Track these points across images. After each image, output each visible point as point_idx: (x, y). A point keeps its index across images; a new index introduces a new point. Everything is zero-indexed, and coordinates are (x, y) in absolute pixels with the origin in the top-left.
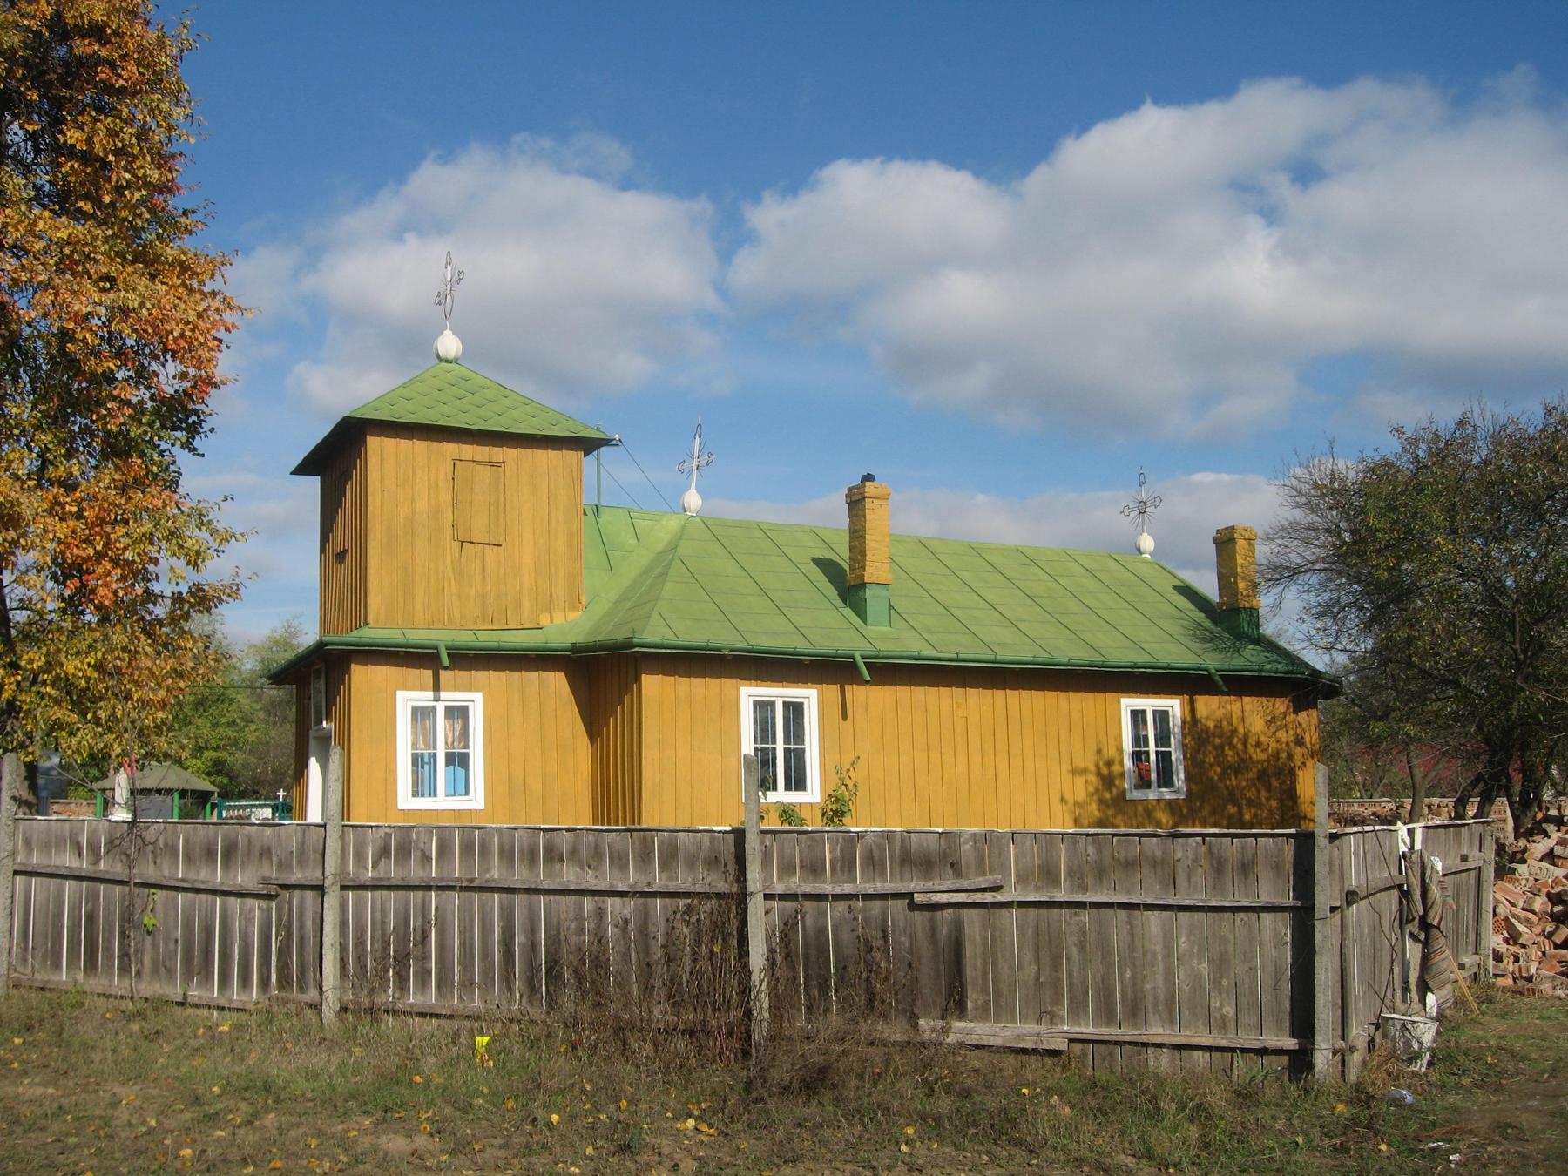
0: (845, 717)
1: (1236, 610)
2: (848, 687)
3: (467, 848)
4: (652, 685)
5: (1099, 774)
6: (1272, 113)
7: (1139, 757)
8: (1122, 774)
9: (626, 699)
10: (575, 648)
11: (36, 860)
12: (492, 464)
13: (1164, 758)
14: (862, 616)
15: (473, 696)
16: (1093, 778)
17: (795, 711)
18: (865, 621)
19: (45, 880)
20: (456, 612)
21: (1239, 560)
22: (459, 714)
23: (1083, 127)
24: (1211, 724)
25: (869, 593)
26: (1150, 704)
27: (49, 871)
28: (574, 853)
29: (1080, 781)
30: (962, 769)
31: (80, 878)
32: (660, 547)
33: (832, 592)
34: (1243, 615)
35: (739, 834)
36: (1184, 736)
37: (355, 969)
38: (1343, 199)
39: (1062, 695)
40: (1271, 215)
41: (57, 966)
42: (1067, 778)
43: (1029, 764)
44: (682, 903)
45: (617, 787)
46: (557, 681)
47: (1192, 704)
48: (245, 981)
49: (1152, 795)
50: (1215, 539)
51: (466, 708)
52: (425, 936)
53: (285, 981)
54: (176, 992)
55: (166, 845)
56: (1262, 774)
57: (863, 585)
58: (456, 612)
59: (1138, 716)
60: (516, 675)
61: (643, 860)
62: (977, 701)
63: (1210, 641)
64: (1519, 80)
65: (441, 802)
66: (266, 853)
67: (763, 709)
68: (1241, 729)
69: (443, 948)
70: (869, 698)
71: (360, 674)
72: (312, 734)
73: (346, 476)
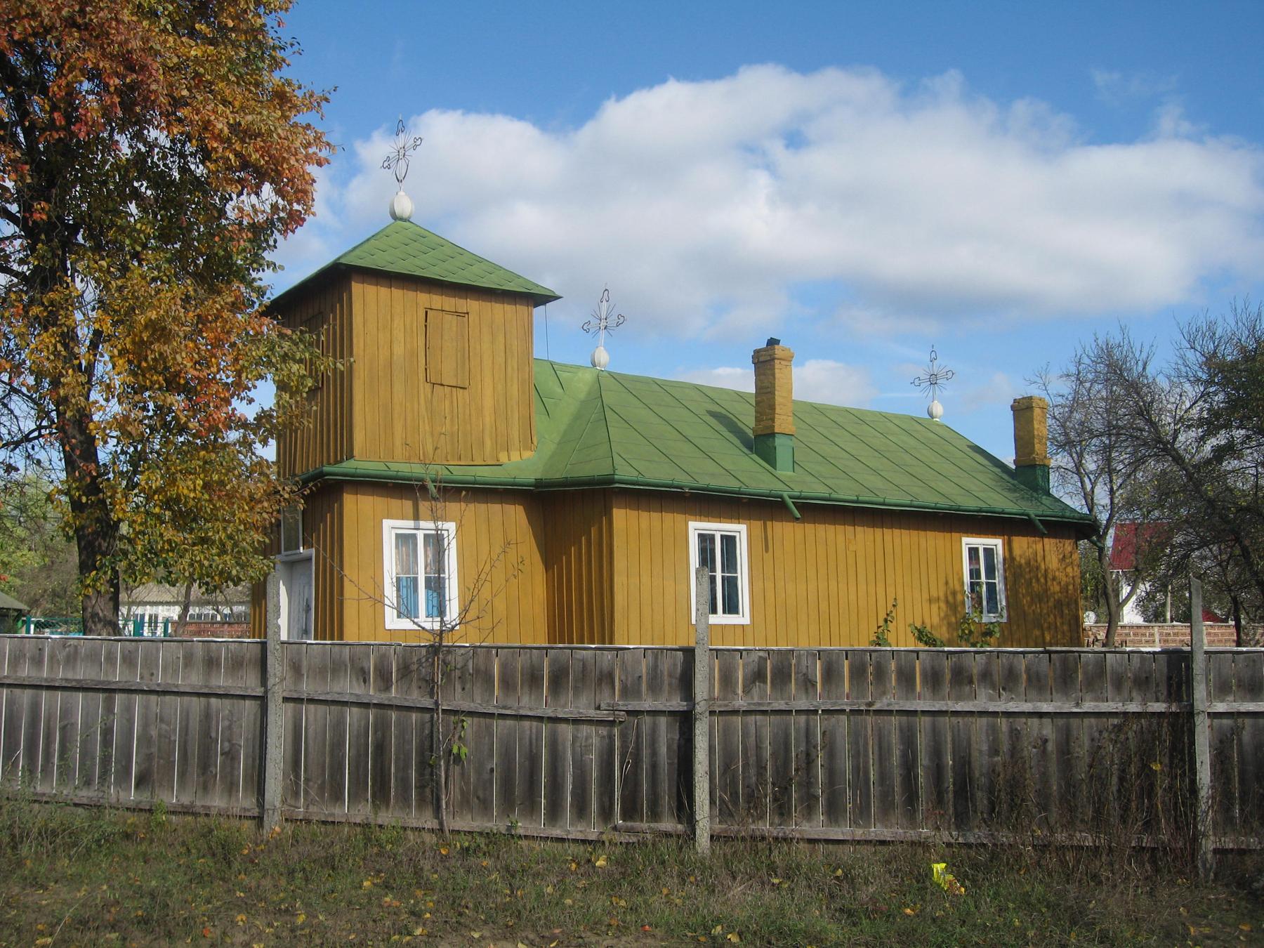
2: (769, 524)
3: (858, 673)
4: (622, 518)
5: (947, 602)
6: (765, 92)
9: (594, 531)
10: (539, 483)
11: (307, 688)
12: (457, 313)
14: (772, 462)
16: (943, 605)
17: (729, 542)
18: (774, 467)
19: (321, 708)
21: (1036, 426)
22: (436, 541)
23: (623, 91)
24: (1023, 561)
25: (779, 441)
26: (981, 542)
27: (329, 698)
29: (935, 607)
30: (853, 597)
32: (582, 396)
33: (737, 442)
34: (1039, 472)
35: (689, 653)
36: (1005, 571)
38: (822, 163)
39: (922, 533)
40: (770, 168)
41: (337, 797)
42: (926, 605)
46: (516, 515)
48: (581, 810)
50: (1012, 407)
52: (809, 760)
53: (631, 811)
54: (496, 824)
55: (477, 671)
56: (1059, 603)
57: (773, 435)
59: (973, 552)
60: (483, 507)
61: (1065, 683)
62: (863, 538)
63: (1015, 491)
64: (952, 80)
66: (606, 678)
69: (831, 773)
70: (786, 532)
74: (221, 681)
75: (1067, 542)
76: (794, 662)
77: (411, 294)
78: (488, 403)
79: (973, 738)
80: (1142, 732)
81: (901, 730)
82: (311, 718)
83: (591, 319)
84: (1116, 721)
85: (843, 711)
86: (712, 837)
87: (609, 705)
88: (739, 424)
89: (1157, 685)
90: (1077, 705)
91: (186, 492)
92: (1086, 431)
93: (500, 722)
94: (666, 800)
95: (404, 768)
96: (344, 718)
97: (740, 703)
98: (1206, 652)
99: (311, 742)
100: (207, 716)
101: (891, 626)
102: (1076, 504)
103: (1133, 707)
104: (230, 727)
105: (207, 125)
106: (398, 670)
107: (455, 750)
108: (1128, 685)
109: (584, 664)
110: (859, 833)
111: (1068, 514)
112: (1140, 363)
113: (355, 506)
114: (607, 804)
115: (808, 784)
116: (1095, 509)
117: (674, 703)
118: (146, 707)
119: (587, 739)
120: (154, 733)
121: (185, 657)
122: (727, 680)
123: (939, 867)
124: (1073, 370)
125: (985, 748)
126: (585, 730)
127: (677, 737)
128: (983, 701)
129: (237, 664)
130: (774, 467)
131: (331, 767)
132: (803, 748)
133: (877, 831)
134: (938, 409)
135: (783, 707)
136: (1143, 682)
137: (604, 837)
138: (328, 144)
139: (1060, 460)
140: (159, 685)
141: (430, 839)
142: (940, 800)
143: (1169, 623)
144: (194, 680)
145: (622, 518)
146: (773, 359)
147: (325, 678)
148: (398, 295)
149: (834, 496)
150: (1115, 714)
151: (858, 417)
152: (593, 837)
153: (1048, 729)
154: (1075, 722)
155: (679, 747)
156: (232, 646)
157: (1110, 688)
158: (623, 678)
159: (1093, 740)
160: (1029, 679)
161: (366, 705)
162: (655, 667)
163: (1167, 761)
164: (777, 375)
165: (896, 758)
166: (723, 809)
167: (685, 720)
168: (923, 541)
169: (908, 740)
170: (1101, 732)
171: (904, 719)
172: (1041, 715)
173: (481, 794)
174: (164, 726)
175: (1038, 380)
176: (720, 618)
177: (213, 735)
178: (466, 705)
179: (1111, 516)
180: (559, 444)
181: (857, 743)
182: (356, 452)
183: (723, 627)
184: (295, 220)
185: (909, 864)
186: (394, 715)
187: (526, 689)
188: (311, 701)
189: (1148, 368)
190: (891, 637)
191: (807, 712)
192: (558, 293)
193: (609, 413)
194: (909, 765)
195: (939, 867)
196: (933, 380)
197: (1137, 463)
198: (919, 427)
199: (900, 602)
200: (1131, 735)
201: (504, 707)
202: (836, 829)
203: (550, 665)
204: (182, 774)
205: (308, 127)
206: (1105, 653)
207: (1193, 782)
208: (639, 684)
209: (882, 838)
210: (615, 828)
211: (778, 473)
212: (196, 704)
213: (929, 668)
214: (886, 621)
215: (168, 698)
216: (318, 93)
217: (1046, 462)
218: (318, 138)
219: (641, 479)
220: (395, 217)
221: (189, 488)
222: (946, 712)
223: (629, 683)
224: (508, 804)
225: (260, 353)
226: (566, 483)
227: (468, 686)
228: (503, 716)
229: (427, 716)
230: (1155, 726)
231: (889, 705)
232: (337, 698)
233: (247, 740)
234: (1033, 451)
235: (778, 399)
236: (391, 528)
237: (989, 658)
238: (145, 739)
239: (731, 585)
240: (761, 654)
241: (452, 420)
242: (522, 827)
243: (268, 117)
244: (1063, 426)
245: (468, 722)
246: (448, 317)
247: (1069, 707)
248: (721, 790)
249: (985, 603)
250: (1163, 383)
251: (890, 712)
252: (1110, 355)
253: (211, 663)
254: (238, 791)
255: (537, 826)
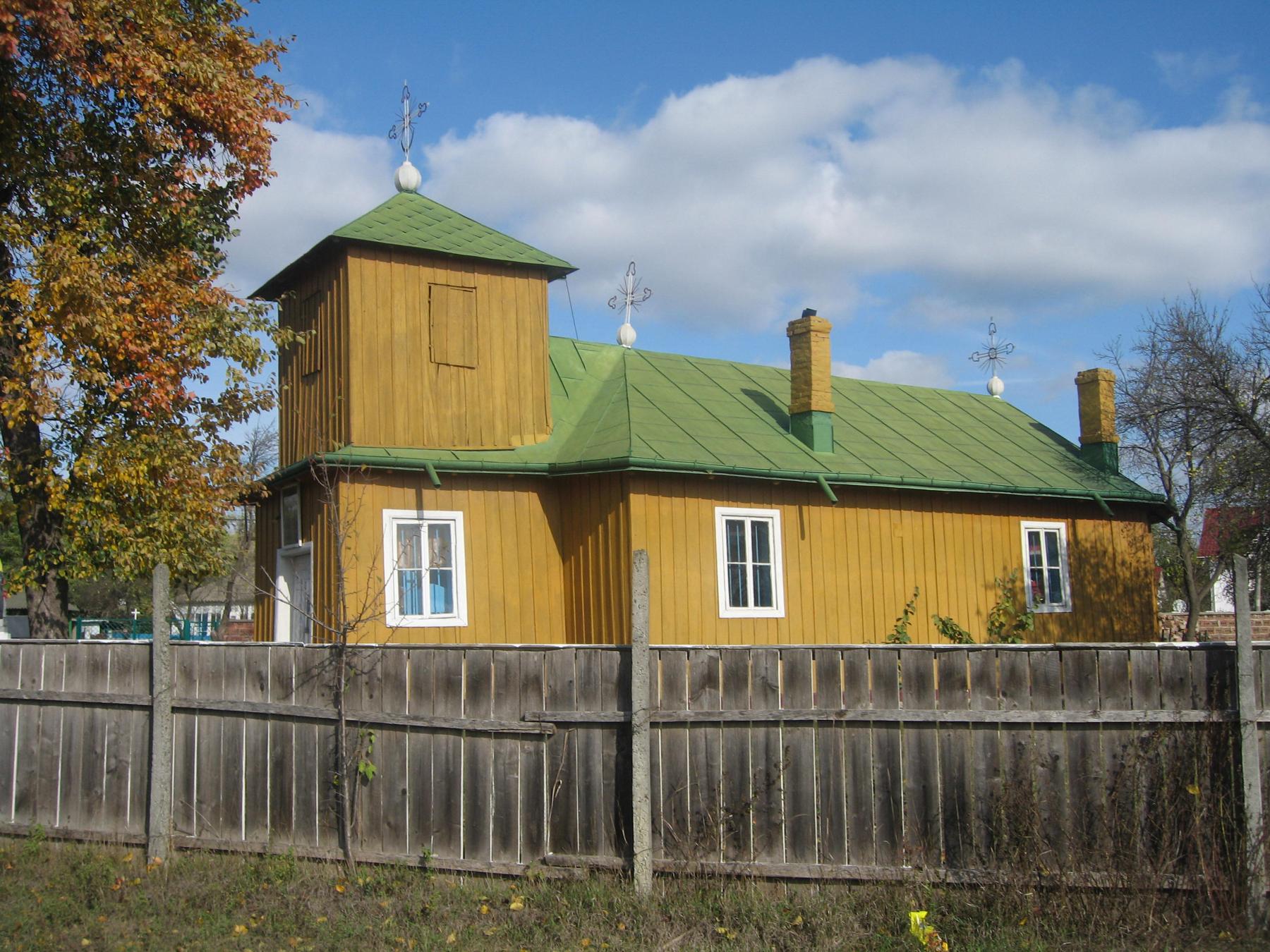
0: (803, 537)
1: (1099, 444)
2: (805, 508)
3: (828, 675)
4: (639, 503)
6: (822, 85)
7: (1036, 574)
8: (1023, 589)
9: (611, 518)
10: (553, 469)
11: (199, 695)
12: (464, 288)
13: (1054, 575)
14: (810, 443)
15: (454, 515)
17: (761, 529)
18: (811, 447)
19: (215, 718)
20: (435, 432)
21: (1102, 400)
22: (441, 533)
23: (683, 87)
24: (1088, 545)
25: (816, 420)
26: (1042, 526)
27: (221, 707)
28: (982, 679)
29: (991, 595)
31: (264, 716)
32: (605, 376)
33: (773, 421)
34: (1106, 449)
37: (680, 826)
38: (881, 155)
39: (976, 517)
41: (234, 823)
43: (952, 581)
44: (1134, 734)
45: (599, 604)
46: (530, 502)
47: (1074, 526)
48: (505, 840)
49: (1045, 609)
50: (1077, 381)
51: (448, 526)
52: (770, 783)
53: (562, 841)
54: (409, 856)
55: (386, 675)
58: (435, 432)
59: (1034, 537)
60: (493, 494)
61: (1080, 686)
62: (911, 522)
63: (1080, 471)
64: (1013, 68)
65: (427, 619)
66: (532, 683)
67: (734, 527)
68: (1110, 550)
69: (797, 799)
70: (823, 517)
71: (349, 492)
72: (279, 552)
73: (318, 297)
74: (108, 688)
75: (1138, 525)
76: (750, 663)
77: (413, 269)
78: (499, 383)
79: (968, 755)
80: (1176, 747)
81: (880, 746)
82: (204, 731)
83: (618, 295)
84: (1145, 734)
85: (809, 723)
86: (655, 872)
87: (534, 715)
88: (777, 403)
89: (1195, 688)
90: (1095, 713)
91: (127, 478)
92: (1165, 408)
93: (413, 735)
94: (603, 832)
95: (306, 790)
96: (240, 731)
97: (687, 711)
98: (1255, 648)
99: (204, 760)
100: (92, 728)
101: (912, 618)
102: (1149, 483)
103: (1164, 716)
104: (116, 742)
105: (135, 73)
106: (298, 675)
107: (361, 769)
108: (1156, 690)
109: (507, 668)
110: (829, 870)
111: (1137, 494)
112: (1214, 330)
113: (352, 497)
114: (535, 833)
115: (768, 811)
116: (1174, 491)
117: (609, 712)
118: (27, 719)
119: (511, 755)
120: (35, 748)
121: (68, 662)
122: (672, 685)
123: (917, 916)
124: (1147, 342)
125: (982, 766)
126: (509, 743)
127: (614, 753)
128: (976, 708)
129: (123, 669)
130: (811, 447)
131: (226, 787)
132: (762, 767)
133: (850, 867)
134: (998, 385)
135: (737, 718)
136: (1176, 685)
137: (530, 873)
138: (289, 99)
139: (1134, 436)
140: (39, 693)
141: (331, 872)
142: (926, 831)
143: (1259, 611)
144: (76, 686)
145: (639, 503)
146: (809, 331)
147: (218, 685)
148: (399, 270)
149: (876, 477)
150: (1137, 725)
151: (911, 395)
152: (518, 872)
153: (1060, 743)
154: (1090, 734)
155: (617, 765)
156: (119, 649)
157: (1135, 692)
158: (551, 683)
159: (1114, 756)
160: (1035, 681)
161: (264, 716)
162: (588, 670)
163: (1207, 782)
164: (813, 349)
165: (873, 776)
166: (666, 838)
167: (623, 732)
168: (977, 526)
169: (889, 756)
170: (1125, 747)
171: (883, 731)
172: (1050, 726)
173: (392, 820)
174: (46, 740)
175: (1110, 354)
176: (752, 611)
177: (99, 750)
178: (372, 716)
179: (1190, 497)
180: (578, 426)
181: (827, 761)
182: (354, 438)
183: (755, 620)
184: (252, 182)
185: (881, 910)
186: (294, 726)
187: (441, 696)
188: (203, 711)
189: (1222, 335)
190: (910, 631)
191: (767, 723)
192: (574, 265)
193: (631, 392)
194: (889, 788)
195: (917, 916)
196: (993, 354)
197: (1216, 438)
198: (976, 404)
199: (921, 591)
200: (1162, 750)
201: (416, 718)
202: (803, 865)
203: (469, 668)
204: (66, 796)
205: (265, 80)
206: (1128, 649)
207: (1241, 809)
208: (571, 690)
209: (857, 877)
210: (544, 862)
211: (816, 454)
212: (81, 714)
213: (912, 670)
214: (906, 612)
215: (50, 708)
216: (276, 42)
217: (1114, 439)
218: (277, 93)
219: (659, 461)
220: (400, 188)
221: (130, 474)
222: (934, 723)
223: (558, 688)
224: (422, 830)
225: (206, 325)
226: (580, 467)
227: (376, 693)
228: (415, 729)
229: (332, 728)
230: (1192, 741)
231: (864, 714)
232: (230, 707)
233: (134, 756)
234: (1099, 427)
235: (815, 374)
236: (393, 518)
237: (986, 657)
238: (26, 755)
239: (763, 576)
240: (712, 653)
241: (459, 402)
242: (438, 857)
243: (210, 68)
244: (1137, 403)
245: (377, 735)
246: (454, 293)
247: (1085, 717)
248: (665, 817)
249: (1047, 591)
250: (1239, 349)
251: (865, 724)
252: (1180, 323)
253: (97, 668)
254: (125, 814)
255: (457, 857)
